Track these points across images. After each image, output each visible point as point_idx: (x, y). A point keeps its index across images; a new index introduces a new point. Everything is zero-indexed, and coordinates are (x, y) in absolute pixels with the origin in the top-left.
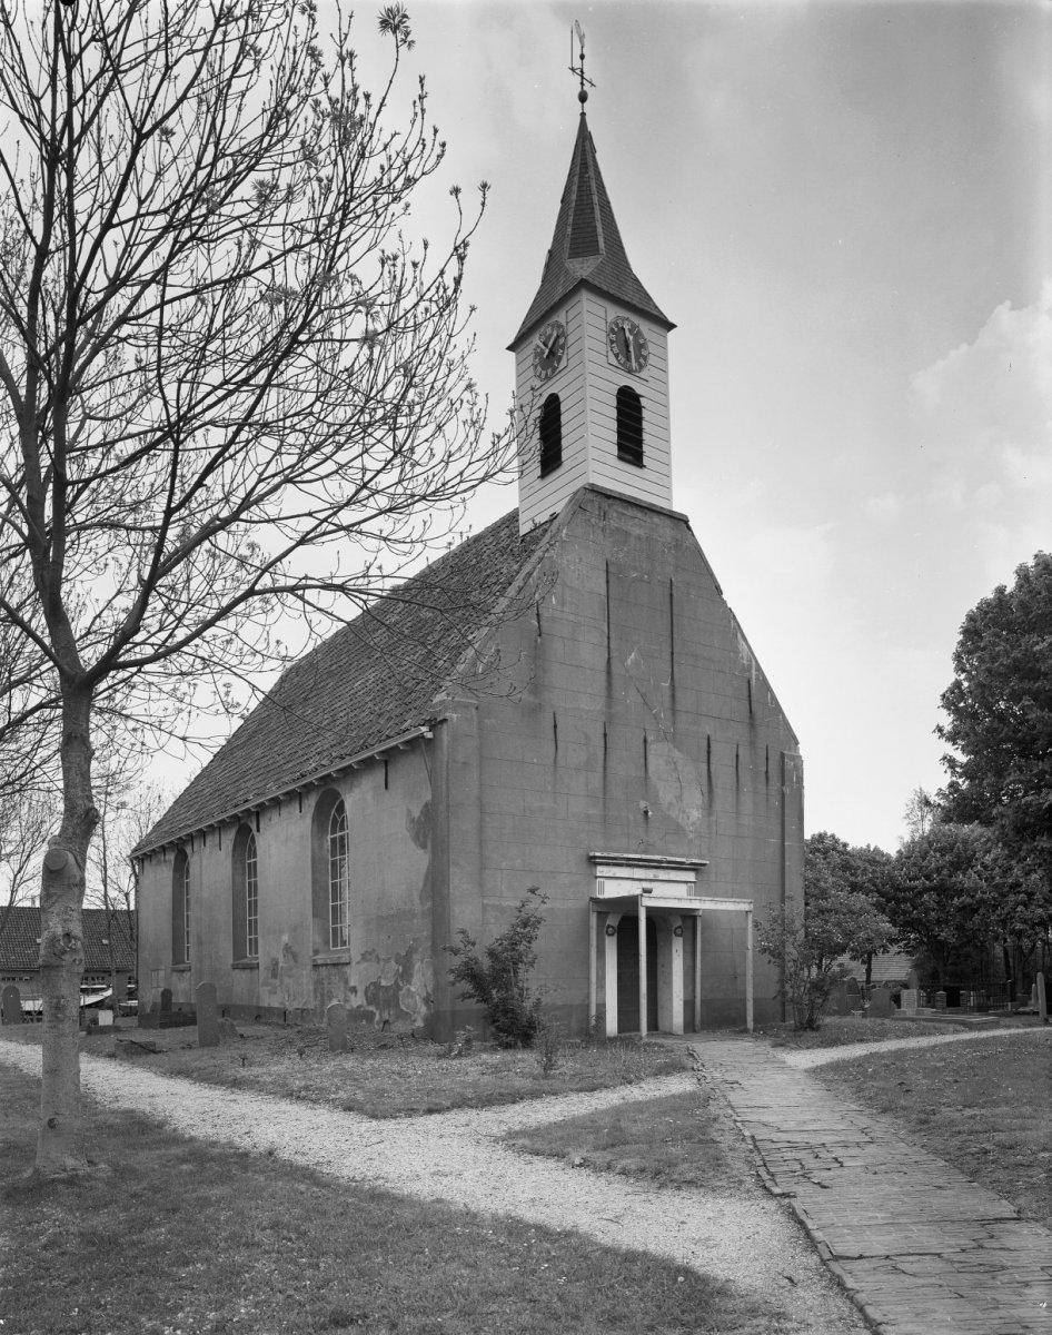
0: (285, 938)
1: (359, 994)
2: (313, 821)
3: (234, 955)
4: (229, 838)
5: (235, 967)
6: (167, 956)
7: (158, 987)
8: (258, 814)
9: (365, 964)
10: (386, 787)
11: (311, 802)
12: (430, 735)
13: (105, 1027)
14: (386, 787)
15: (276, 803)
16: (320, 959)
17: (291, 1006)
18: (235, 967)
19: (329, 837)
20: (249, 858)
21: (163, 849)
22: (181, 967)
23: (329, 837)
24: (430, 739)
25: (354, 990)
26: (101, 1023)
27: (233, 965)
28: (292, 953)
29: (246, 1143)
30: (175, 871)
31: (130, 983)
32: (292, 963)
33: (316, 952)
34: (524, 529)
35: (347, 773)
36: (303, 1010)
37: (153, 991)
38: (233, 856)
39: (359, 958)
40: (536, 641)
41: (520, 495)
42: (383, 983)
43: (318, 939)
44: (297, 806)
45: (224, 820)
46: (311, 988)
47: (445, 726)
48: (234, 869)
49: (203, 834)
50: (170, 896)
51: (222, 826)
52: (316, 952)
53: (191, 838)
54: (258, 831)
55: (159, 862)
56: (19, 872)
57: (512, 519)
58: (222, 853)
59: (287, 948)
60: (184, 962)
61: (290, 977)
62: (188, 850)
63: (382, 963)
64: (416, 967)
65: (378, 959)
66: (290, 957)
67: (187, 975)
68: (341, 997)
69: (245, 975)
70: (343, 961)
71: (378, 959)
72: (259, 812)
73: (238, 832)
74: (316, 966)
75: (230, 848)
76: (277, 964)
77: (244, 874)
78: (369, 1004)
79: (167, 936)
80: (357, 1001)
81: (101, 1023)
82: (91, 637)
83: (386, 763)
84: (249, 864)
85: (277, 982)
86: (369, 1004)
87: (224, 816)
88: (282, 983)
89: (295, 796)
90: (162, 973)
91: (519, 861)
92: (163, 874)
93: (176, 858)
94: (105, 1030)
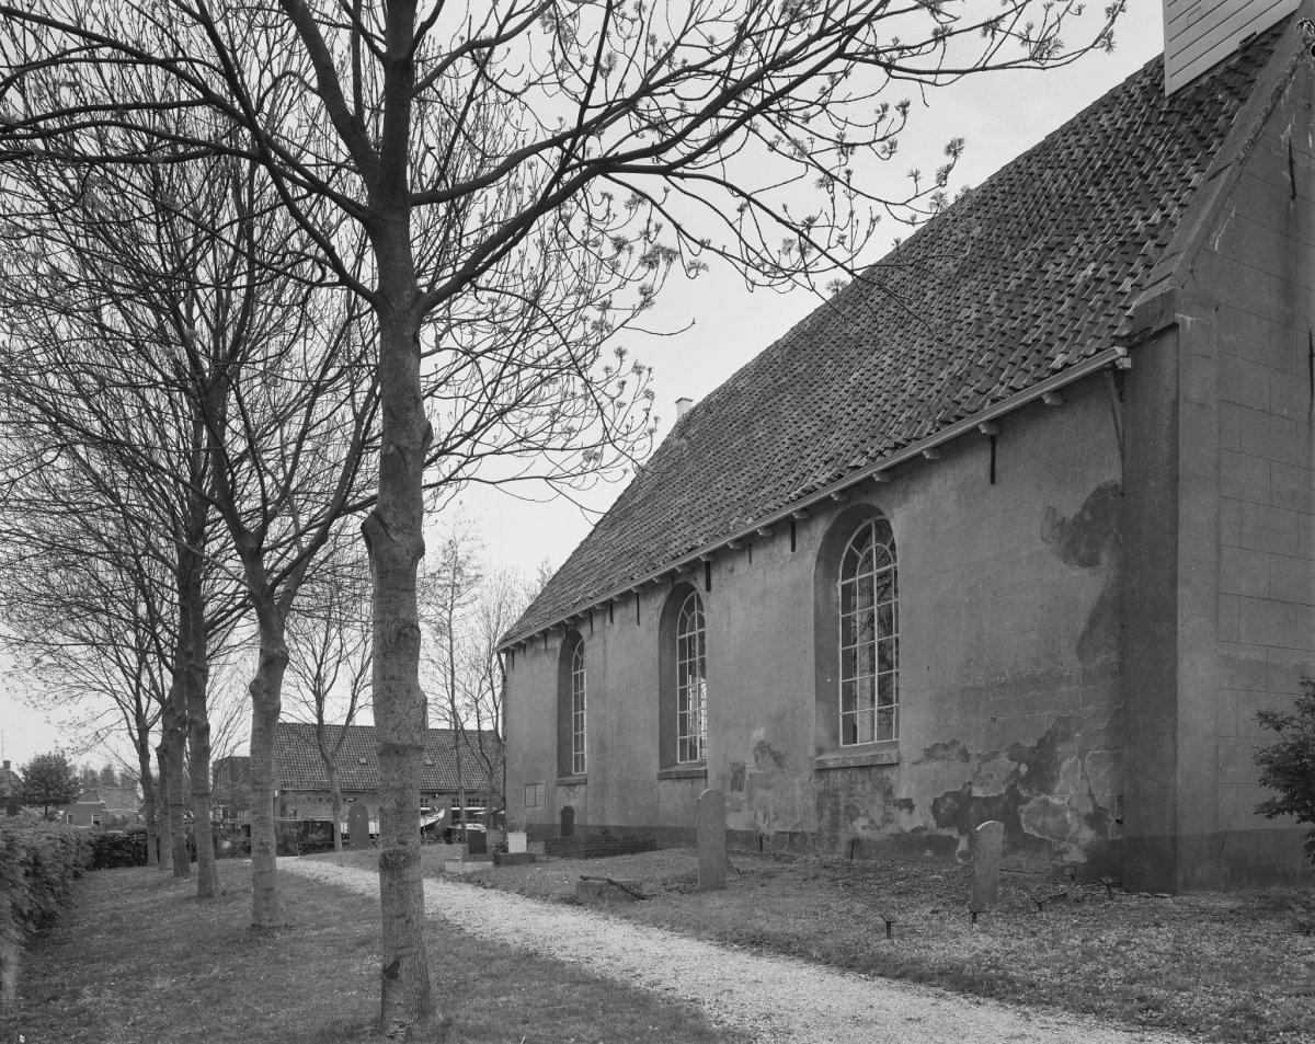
0: (759, 734)
1: (916, 811)
2: (819, 559)
3: (661, 760)
4: (654, 607)
5: (662, 777)
6: (550, 767)
7: (536, 805)
8: (708, 565)
9: (934, 765)
10: (993, 481)
11: (658, 601)
12: (1127, 363)
13: (517, 855)
14: (993, 481)
15: (748, 544)
16: (830, 759)
17: (769, 828)
18: (662, 777)
19: (840, 583)
20: (576, 669)
21: (545, 634)
22: (570, 779)
23: (840, 583)
24: (1125, 371)
25: (908, 804)
26: (512, 849)
27: (659, 774)
28: (772, 753)
29: (560, 956)
30: (562, 660)
31: (422, 806)
32: (772, 767)
33: (820, 751)
34: (1171, 85)
35: (908, 471)
36: (793, 835)
37: (528, 810)
38: (660, 629)
39: (918, 755)
40: (1288, 208)
41: (1167, 32)
42: (978, 792)
43: (823, 732)
44: (787, 544)
45: (577, 615)
46: (812, 802)
47: (1170, 339)
48: (661, 647)
49: (609, 606)
50: (556, 691)
51: (647, 589)
52: (820, 751)
53: (590, 614)
54: (708, 588)
55: (537, 653)
56: (360, 675)
57: (1156, 68)
58: (641, 631)
59: (762, 747)
60: (570, 774)
61: (768, 787)
62: (584, 631)
63: (974, 763)
64: (1065, 765)
65: (965, 756)
66: (769, 759)
67: (581, 790)
68: (877, 814)
69: (683, 787)
70: (885, 760)
71: (965, 756)
72: (707, 565)
73: (669, 599)
74: (822, 771)
75: (656, 619)
76: (742, 770)
77: (673, 654)
78: (941, 824)
79: (550, 743)
80: (920, 818)
81: (512, 849)
82: (567, 177)
83: (993, 440)
84: (682, 642)
85: (742, 796)
86: (941, 824)
87: (652, 575)
88: (750, 798)
89: (788, 527)
90: (540, 789)
91: (1262, 582)
92: (543, 668)
93: (563, 644)
94: (517, 860)
